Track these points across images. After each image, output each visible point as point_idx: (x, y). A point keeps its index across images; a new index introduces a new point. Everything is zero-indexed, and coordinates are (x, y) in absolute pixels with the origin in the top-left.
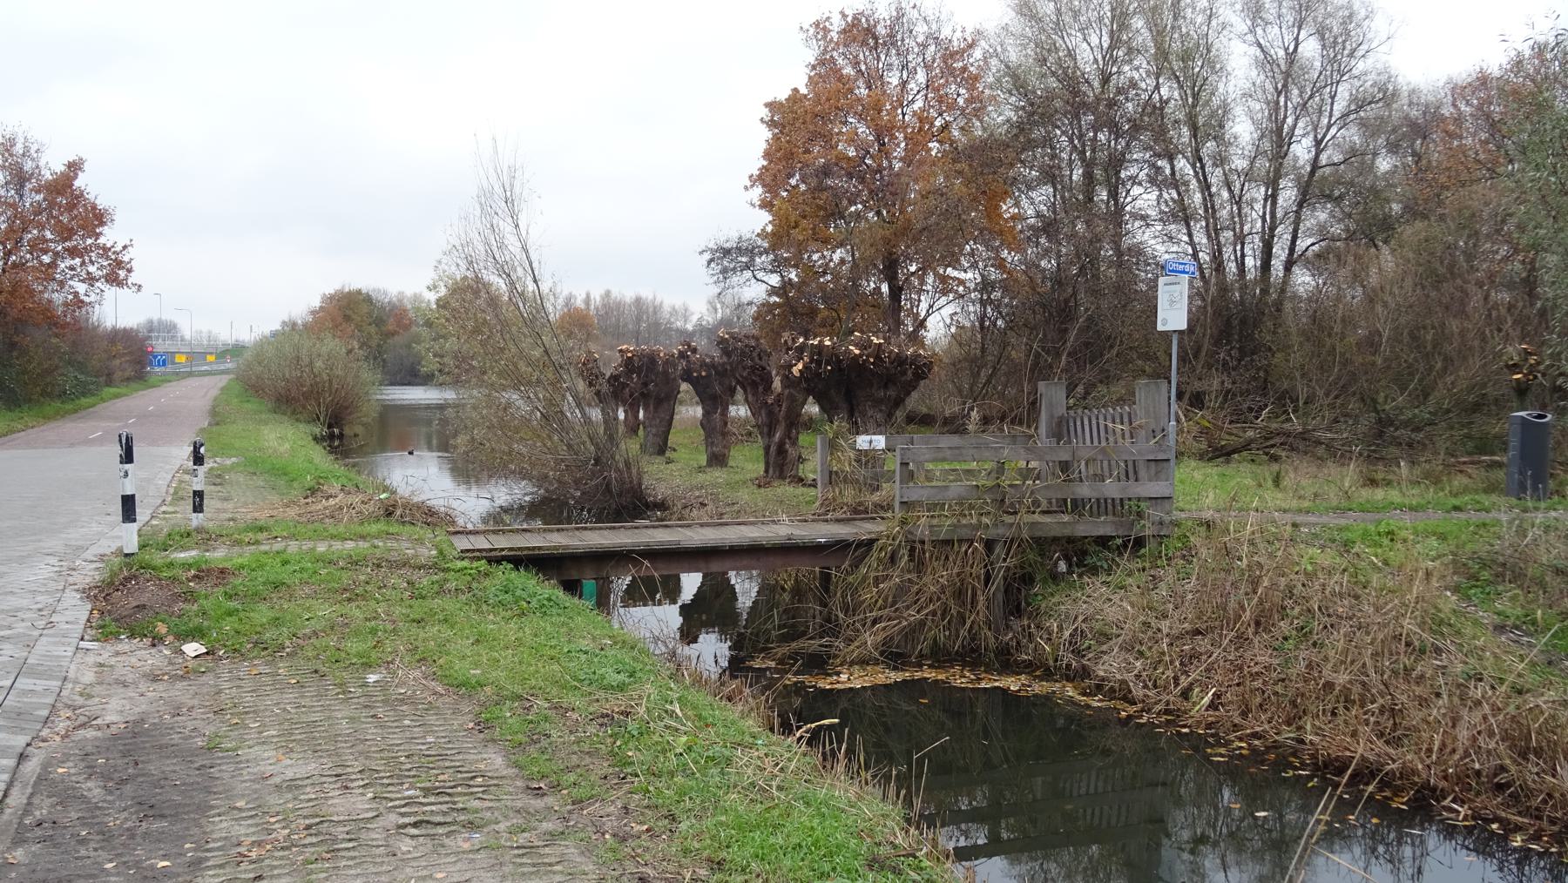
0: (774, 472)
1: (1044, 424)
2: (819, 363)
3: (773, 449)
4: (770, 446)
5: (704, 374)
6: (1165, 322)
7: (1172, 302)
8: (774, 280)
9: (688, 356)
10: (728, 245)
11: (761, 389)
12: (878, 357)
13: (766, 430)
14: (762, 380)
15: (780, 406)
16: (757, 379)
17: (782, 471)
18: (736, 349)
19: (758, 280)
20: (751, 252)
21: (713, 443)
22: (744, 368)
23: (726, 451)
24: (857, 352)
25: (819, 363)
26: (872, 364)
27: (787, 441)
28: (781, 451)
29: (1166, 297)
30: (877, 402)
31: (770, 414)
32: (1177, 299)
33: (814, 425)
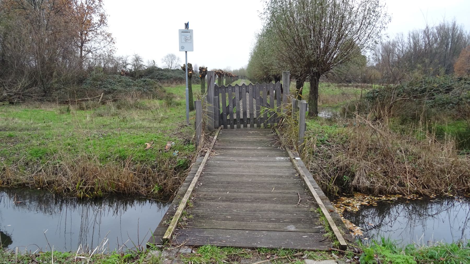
32: (189, 39)
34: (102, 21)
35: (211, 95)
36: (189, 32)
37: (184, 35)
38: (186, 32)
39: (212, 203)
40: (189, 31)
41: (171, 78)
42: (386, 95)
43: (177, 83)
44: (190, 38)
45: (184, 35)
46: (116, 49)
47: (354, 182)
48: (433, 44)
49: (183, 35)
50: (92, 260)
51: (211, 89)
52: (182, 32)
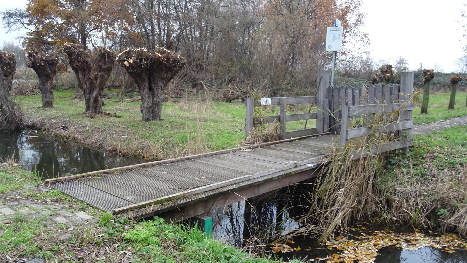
0: (92, 110)
1: (322, 91)
2: (141, 60)
3: (92, 100)
4: (90, 99)
5: (43, 64)
6: (330, 47)
7: (334, 38)
8: (32, 28)
9: (34, 55)
10: (11, 12)
11: (87, 72)
12: (168, 59)
13: (88, 91)
14: (87, 68)
15: (96, 80)
16: (85, 67)
17: (96, 110)
18: (75, 52)
19: (26, 28)
20: (22, 16)
21: (46, 96)
22: (78, 62)
23: (52, 100)
24: (160, 55)
25: (141, 60)
26: (166, 61)
27: (99, 96)
28: (96, 100)
29: (331, 36)
30: (163, 79)
31: (91, 84)
32: (337, 37)
33: (56, 88)
34: (359, 21)
35: (321, 97)
36: (338, 30)
37: (332, 34)
38: (335, 30)
39: (312, 153)
40: (337, 29)
41: (438, 83)
42: (204, 113)
43: (445, 89)
44: (339, 36)
45: (332, 34)
46: (371, 50)
47: (451, 220)
48: (205, 9)
49: (331, 34)
50: (167, 123)
51: (321, 90)
52: (331, 30)
